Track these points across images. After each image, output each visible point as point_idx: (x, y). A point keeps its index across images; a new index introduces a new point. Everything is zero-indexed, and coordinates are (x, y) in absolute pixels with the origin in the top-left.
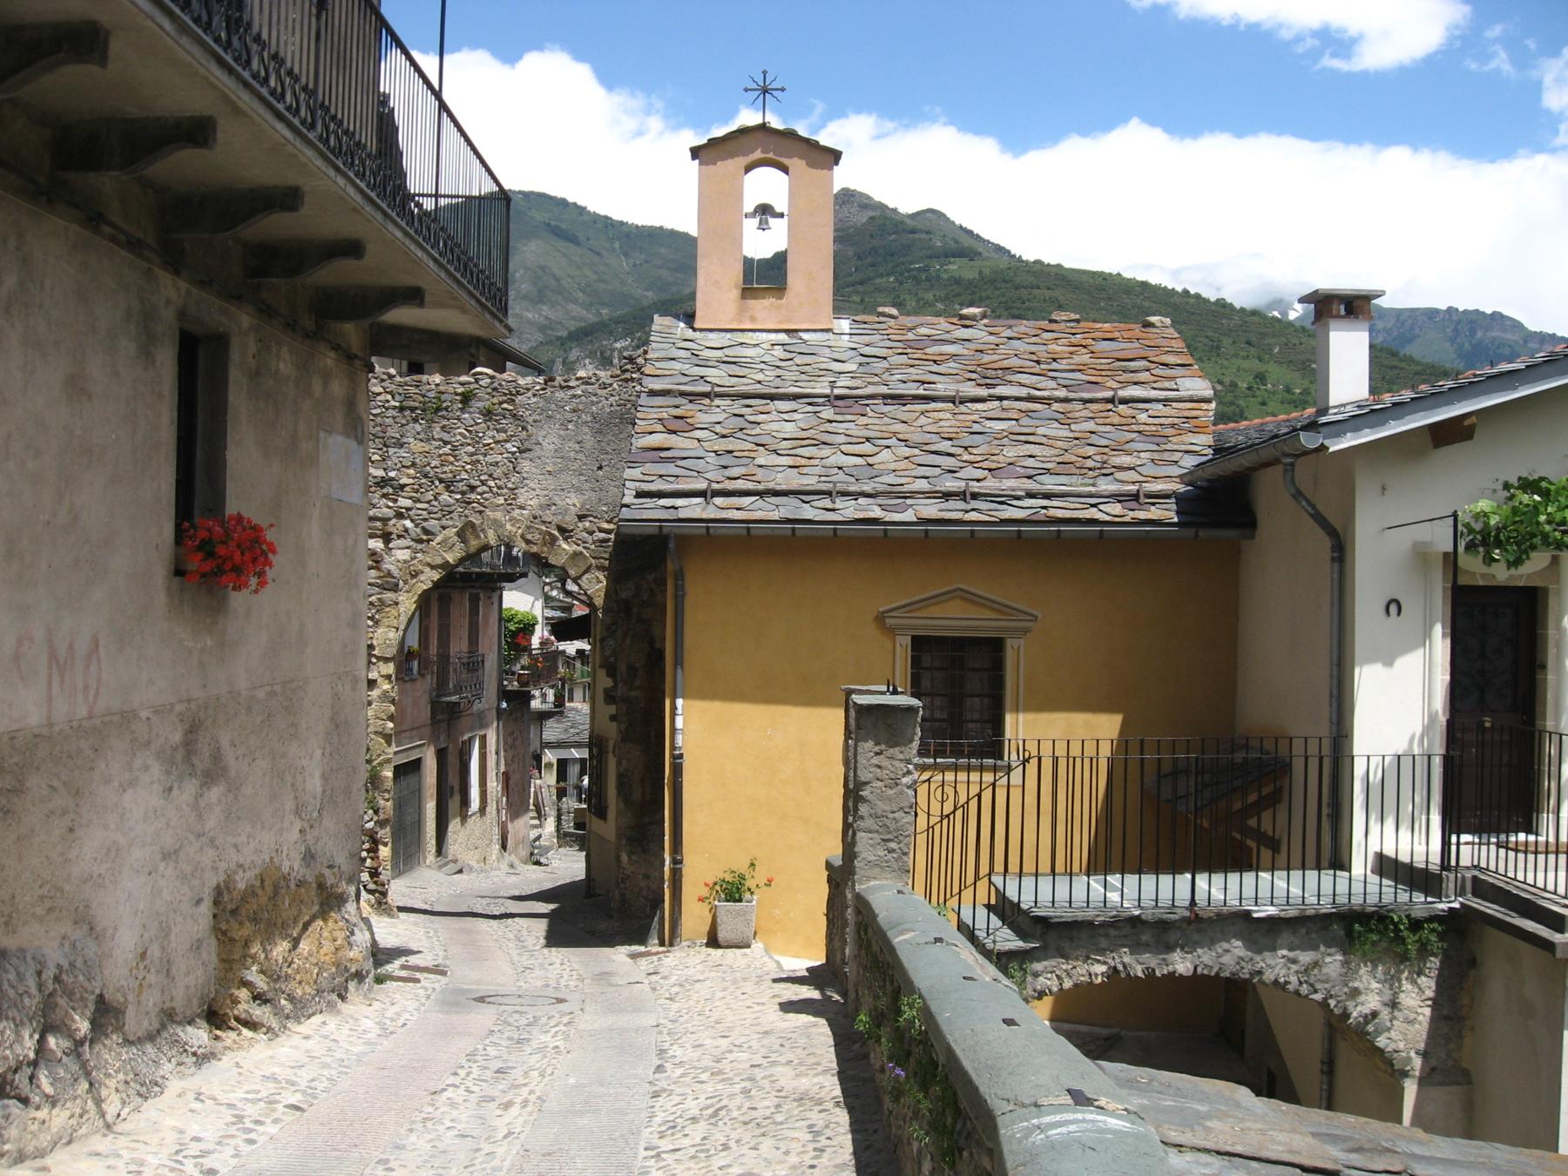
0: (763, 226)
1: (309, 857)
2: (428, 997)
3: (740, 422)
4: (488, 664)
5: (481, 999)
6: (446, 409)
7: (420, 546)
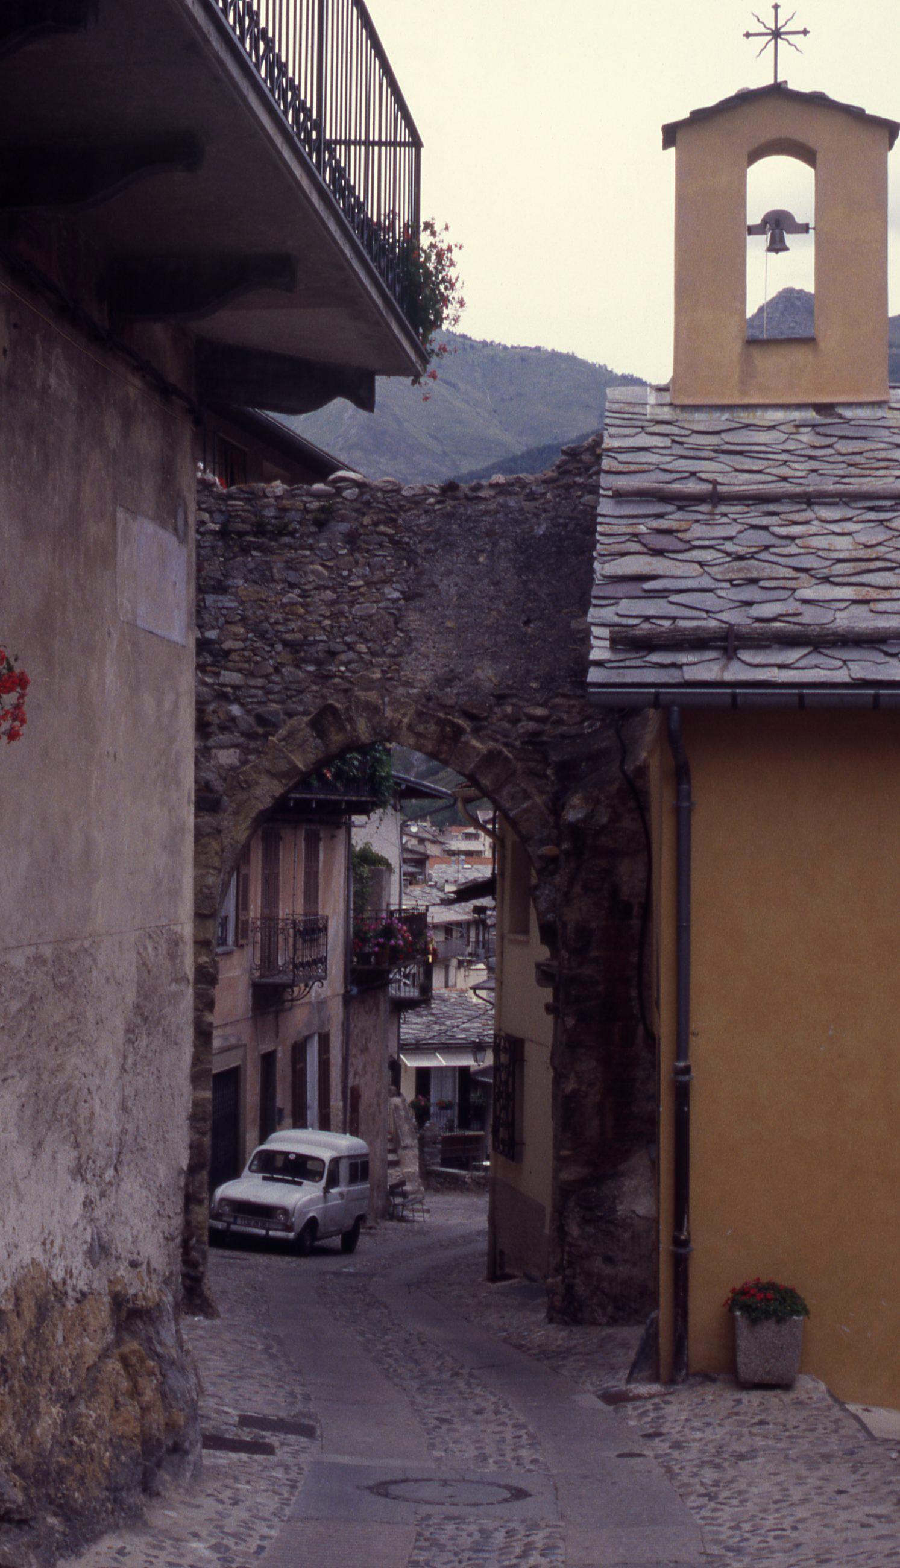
0: (777, 246)
1: (99, 1251)
2: (293, 1486)
3: (764, 538)
4: (331, 931)
5: (382, 1489)
6: (292, 534)
7: (253, 745)
